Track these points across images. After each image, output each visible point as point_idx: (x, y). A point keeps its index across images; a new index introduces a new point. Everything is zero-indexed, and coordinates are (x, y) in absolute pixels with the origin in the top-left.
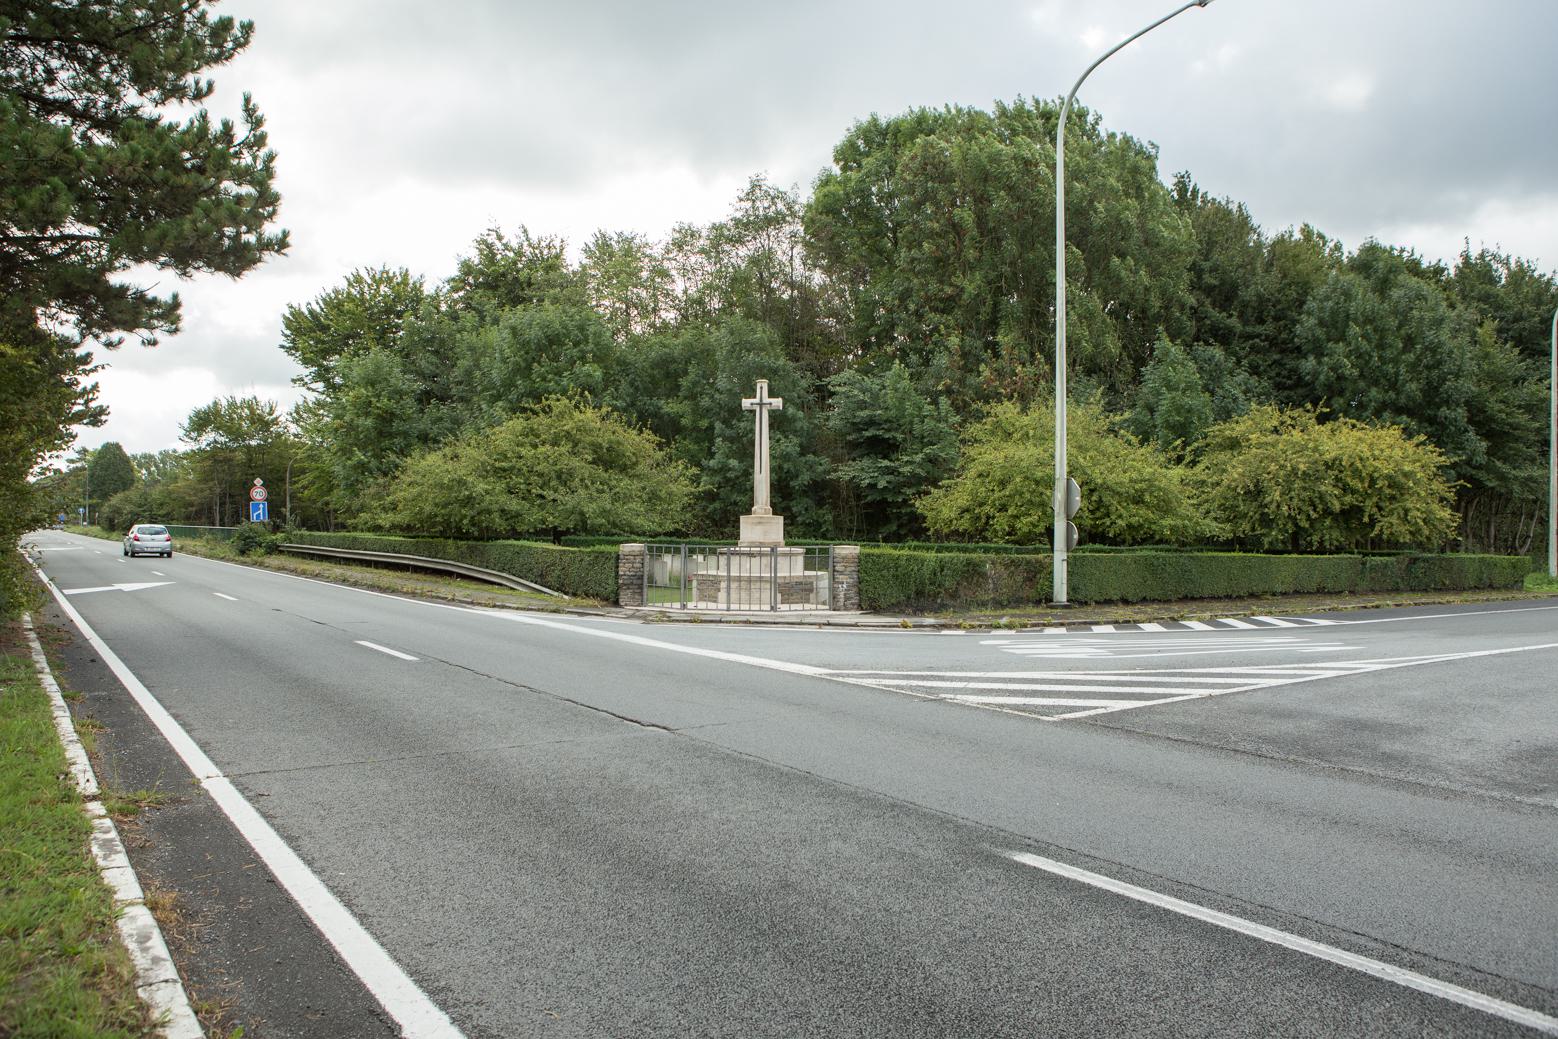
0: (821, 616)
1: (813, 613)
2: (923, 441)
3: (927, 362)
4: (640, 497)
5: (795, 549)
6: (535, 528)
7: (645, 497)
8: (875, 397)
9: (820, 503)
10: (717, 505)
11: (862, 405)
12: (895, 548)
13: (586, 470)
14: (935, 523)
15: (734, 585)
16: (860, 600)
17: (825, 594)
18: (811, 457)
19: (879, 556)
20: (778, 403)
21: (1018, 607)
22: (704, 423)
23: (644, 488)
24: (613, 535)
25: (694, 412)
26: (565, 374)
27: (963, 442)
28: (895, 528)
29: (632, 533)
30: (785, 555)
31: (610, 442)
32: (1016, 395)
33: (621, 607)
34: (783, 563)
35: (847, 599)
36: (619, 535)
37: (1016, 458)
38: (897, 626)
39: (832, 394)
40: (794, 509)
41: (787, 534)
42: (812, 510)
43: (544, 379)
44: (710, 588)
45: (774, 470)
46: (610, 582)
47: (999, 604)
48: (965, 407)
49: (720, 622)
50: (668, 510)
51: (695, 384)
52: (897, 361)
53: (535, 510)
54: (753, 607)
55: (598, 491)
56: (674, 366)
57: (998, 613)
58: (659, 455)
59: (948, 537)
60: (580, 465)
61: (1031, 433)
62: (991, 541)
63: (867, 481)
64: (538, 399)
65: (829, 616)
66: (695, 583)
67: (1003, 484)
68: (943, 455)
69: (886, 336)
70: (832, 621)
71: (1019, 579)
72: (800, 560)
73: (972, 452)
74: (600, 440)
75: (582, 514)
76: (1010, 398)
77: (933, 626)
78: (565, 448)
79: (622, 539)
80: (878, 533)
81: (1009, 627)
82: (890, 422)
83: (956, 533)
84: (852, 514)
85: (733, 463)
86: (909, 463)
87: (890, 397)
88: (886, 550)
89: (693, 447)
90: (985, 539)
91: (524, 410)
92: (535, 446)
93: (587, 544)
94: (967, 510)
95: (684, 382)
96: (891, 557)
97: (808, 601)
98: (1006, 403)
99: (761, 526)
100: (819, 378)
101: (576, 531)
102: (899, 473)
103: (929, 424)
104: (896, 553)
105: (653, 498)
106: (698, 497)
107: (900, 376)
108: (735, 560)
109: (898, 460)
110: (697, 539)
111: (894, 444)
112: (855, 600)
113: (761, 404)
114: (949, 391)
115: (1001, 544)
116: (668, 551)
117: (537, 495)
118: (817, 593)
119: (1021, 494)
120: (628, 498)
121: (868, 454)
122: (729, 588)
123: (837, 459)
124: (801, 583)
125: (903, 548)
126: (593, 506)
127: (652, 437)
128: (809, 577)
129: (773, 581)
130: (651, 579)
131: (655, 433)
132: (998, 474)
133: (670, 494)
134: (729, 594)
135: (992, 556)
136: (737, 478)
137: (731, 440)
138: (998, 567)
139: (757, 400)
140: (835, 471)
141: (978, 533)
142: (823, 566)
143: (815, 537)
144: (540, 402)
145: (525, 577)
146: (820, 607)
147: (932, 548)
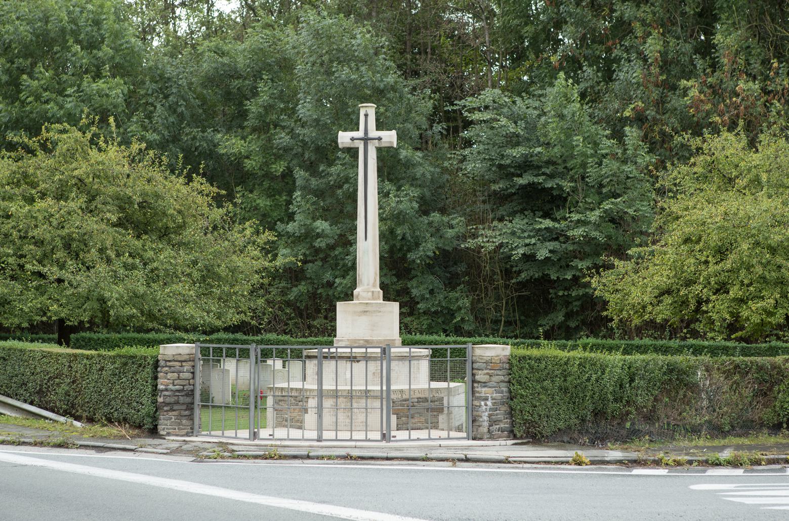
0: (456, 448)
1: (443, 443)
2: (602, 191)
3: (609, 76)
4: (189, 275)
5: (416, 351)
6: (30, 321)
7: (196, 275)
8: (531, 127)
9: (451, 283)
10: (303, 287)
11: (513, 140)
12: (563, 347)
13: (109, 236)
14: (621, 311)
15: (328, 403)
16: (513, 424)
17: (460, 416)
18: (436, 216)
19: (539, 360)
20: (390, 137)
21: (746, 435)
22: (279, 168)
23: (195, 263)
24: (148, 331)
25: (266, 149)
26: (70, 91)
27: (661, 192)
28: (561, 318)
29: (177, 328)
30: (402, 358)
31: (144, 194)
32: (741, 123)
33: (161, 437)
34: (399, 370)
35: (492, 422)
36: (158, 331)
37: (741, 214)
38: (567, 463)
39: (468, 124)
40: (415, 292)
41: (405, 328)
42: (443, 295)
43: (38, 98)
44: (292, 406)
45: (385, 236)
46: (144, 400)
47: (717, 431)
48: (663, 142)
49: (308, 457)
50: (230, 295)
51: (268, 108)
52: (562, 75)
53: (31, 295)
54: (356, 436)
55: (126, 266)
56: (236, 83)
57: (716, 443)
58: (217, 214)
59: (639, 331)
60: (99, 228)
61: (764, 177)
62: (704, 337)
63: (521, 251)
64: (34, 130)
65: (468, 448)
66: (270, 401)
67: (721, 253)
68: (631, 211)
69: (546, 38)
70: (471, 454)
71: (747, 392)
72: (424, 367)
73: (675, 207)
74: (129, 192)
75: (102, 300)
76: (732, 126)
77: (620, 462)
78: (75, 203)
79: (162, 336)
80: (537, 327)
81: (734, 463)
82: (554, 163)
83: (651, 324)
84: (498, 298)
85: (322, 225)
86: (583, 222)
87: (553, 129)
88: (550, 350)
89: (263, 202)
90: (695, 334)
91: (11, 147)
92: (31, 200)
93: (112, 345)
94: (668, 292)
95: (253, 107)
96: (557, 362)
97: (435, 426)
98: (725, 134)
99: (367, 317)
100: (450, 100)
101: (93, 325)
102: (567, 238)
103: (610, 166)
104: (563, 354)
105: (209, 277)
106: (275, 275)
107: (565, 95)
108: (329, 367)
109: (565, 219)
110: (272, 336)
111: (559, 197)
112: (505, 424)
113: (366, 140)
114: (640, 119)
115: (720, 341)
116: (231, 354)
117: (33, 273)
118: (449, 413)
119: (749, 268)
120: (171, 277)
121: (522, 211)
122: (320, 408)
123: (475, 219)
124: (426, 400)
125: (574, 347)
126: (115, 286)
127: (207, 188)
128: (437, 390)
129: (386, 396)
130: (206, 396)
131: (211, 181)
132: (714, 239)
133: (233, 270)
134: (320, 416)
135: (706, 358)
136: (332, 248)
137: (319, 194)
138: (716, 375)
139: (360, 134)
140: (474, 236)
141: (686, 324)
142: (458, 375)
143: (445, 331)
144: (37, 132)
145: (16, 396)
146: (453, 434)
147: (617, 348)
